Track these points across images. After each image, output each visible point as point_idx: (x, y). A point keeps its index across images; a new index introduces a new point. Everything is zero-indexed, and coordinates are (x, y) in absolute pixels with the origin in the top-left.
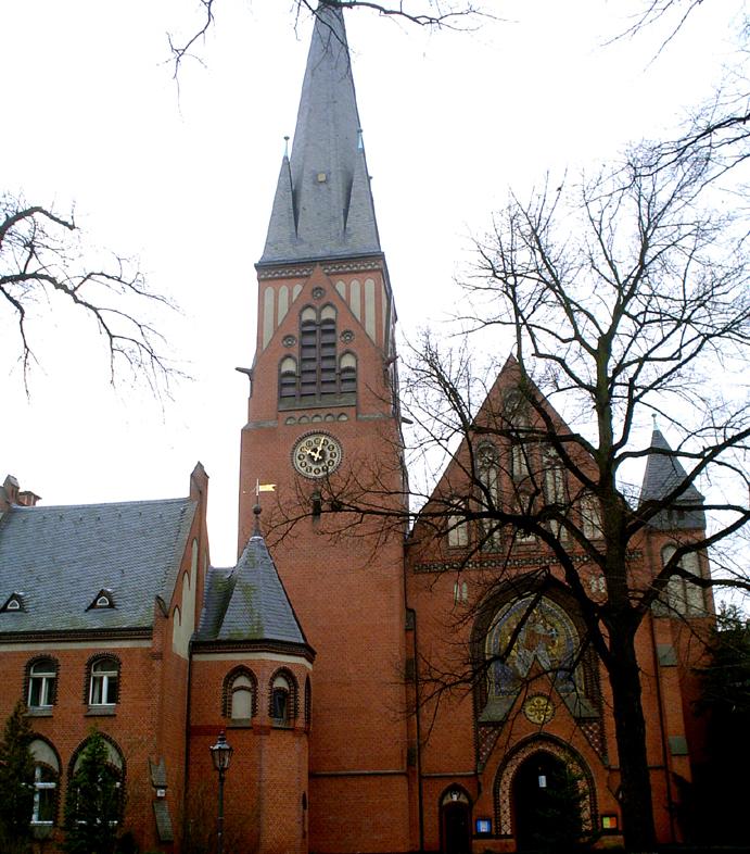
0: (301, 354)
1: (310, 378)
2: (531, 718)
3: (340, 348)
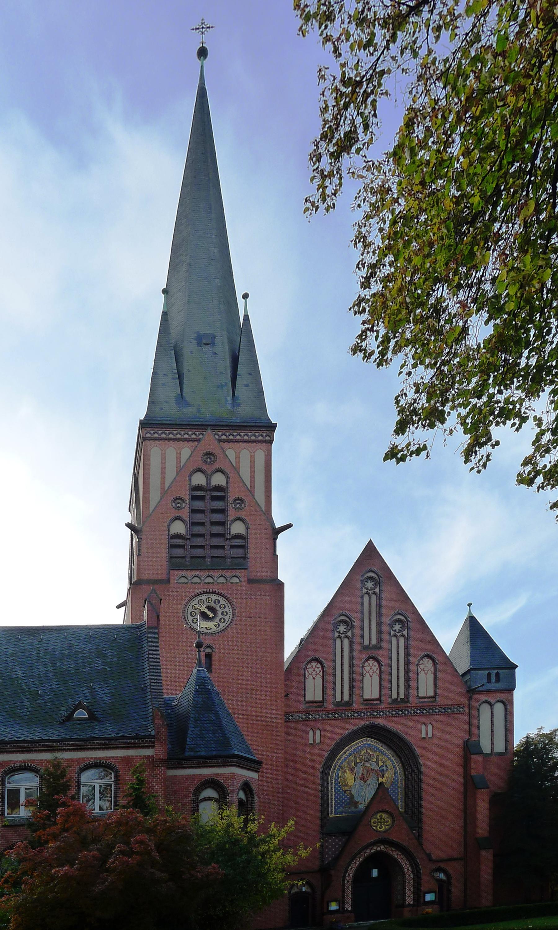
0: (190, 518)
1: (199, 541)
2: (375, 828)
3: (232, 514)
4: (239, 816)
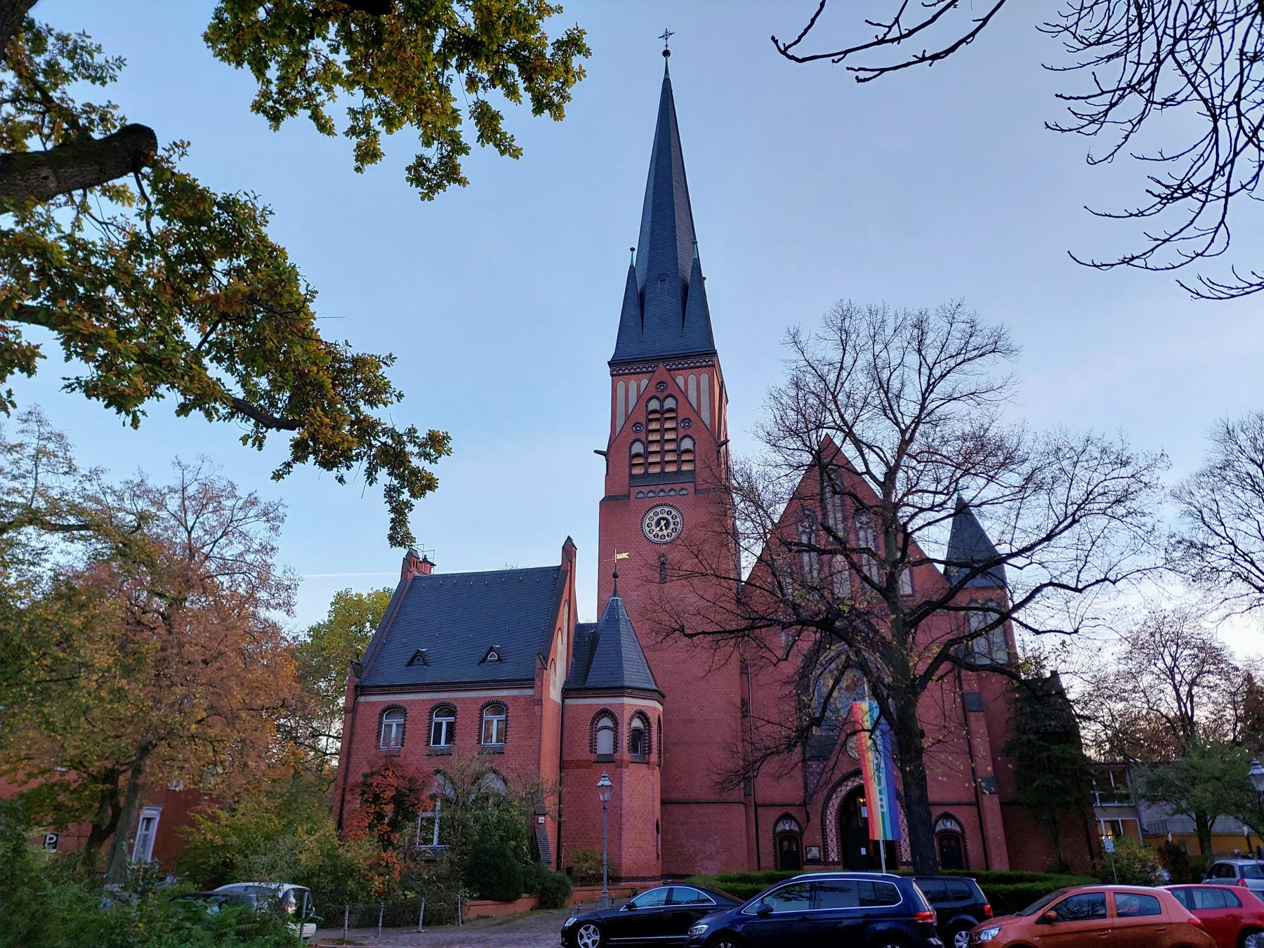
4: (1055, 674)
